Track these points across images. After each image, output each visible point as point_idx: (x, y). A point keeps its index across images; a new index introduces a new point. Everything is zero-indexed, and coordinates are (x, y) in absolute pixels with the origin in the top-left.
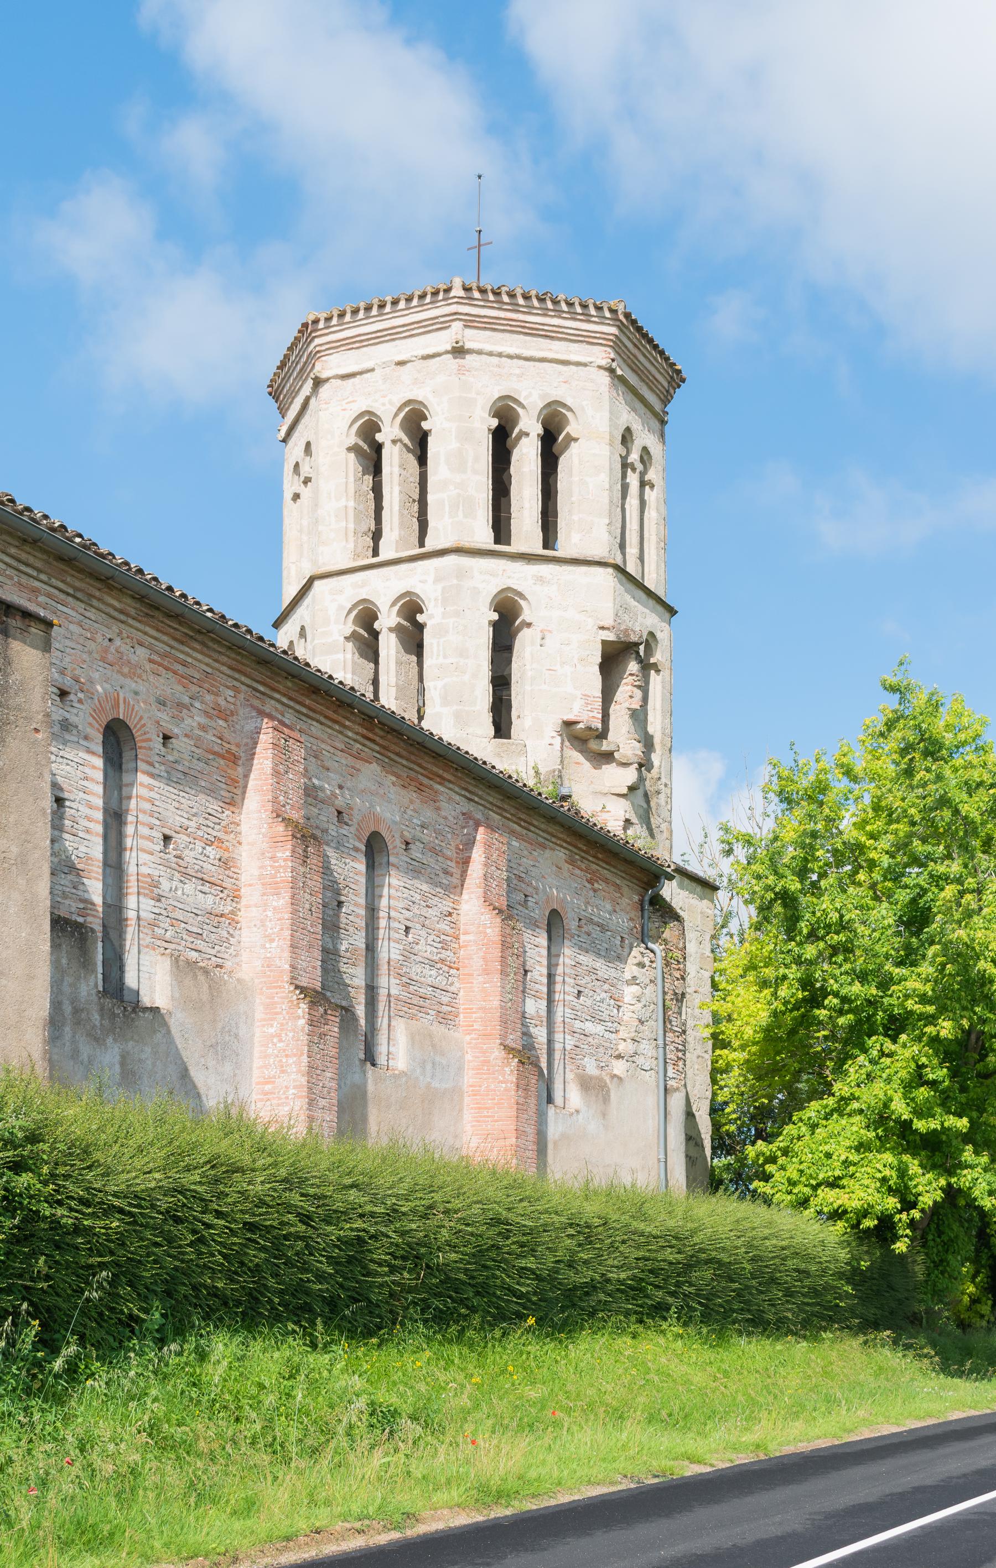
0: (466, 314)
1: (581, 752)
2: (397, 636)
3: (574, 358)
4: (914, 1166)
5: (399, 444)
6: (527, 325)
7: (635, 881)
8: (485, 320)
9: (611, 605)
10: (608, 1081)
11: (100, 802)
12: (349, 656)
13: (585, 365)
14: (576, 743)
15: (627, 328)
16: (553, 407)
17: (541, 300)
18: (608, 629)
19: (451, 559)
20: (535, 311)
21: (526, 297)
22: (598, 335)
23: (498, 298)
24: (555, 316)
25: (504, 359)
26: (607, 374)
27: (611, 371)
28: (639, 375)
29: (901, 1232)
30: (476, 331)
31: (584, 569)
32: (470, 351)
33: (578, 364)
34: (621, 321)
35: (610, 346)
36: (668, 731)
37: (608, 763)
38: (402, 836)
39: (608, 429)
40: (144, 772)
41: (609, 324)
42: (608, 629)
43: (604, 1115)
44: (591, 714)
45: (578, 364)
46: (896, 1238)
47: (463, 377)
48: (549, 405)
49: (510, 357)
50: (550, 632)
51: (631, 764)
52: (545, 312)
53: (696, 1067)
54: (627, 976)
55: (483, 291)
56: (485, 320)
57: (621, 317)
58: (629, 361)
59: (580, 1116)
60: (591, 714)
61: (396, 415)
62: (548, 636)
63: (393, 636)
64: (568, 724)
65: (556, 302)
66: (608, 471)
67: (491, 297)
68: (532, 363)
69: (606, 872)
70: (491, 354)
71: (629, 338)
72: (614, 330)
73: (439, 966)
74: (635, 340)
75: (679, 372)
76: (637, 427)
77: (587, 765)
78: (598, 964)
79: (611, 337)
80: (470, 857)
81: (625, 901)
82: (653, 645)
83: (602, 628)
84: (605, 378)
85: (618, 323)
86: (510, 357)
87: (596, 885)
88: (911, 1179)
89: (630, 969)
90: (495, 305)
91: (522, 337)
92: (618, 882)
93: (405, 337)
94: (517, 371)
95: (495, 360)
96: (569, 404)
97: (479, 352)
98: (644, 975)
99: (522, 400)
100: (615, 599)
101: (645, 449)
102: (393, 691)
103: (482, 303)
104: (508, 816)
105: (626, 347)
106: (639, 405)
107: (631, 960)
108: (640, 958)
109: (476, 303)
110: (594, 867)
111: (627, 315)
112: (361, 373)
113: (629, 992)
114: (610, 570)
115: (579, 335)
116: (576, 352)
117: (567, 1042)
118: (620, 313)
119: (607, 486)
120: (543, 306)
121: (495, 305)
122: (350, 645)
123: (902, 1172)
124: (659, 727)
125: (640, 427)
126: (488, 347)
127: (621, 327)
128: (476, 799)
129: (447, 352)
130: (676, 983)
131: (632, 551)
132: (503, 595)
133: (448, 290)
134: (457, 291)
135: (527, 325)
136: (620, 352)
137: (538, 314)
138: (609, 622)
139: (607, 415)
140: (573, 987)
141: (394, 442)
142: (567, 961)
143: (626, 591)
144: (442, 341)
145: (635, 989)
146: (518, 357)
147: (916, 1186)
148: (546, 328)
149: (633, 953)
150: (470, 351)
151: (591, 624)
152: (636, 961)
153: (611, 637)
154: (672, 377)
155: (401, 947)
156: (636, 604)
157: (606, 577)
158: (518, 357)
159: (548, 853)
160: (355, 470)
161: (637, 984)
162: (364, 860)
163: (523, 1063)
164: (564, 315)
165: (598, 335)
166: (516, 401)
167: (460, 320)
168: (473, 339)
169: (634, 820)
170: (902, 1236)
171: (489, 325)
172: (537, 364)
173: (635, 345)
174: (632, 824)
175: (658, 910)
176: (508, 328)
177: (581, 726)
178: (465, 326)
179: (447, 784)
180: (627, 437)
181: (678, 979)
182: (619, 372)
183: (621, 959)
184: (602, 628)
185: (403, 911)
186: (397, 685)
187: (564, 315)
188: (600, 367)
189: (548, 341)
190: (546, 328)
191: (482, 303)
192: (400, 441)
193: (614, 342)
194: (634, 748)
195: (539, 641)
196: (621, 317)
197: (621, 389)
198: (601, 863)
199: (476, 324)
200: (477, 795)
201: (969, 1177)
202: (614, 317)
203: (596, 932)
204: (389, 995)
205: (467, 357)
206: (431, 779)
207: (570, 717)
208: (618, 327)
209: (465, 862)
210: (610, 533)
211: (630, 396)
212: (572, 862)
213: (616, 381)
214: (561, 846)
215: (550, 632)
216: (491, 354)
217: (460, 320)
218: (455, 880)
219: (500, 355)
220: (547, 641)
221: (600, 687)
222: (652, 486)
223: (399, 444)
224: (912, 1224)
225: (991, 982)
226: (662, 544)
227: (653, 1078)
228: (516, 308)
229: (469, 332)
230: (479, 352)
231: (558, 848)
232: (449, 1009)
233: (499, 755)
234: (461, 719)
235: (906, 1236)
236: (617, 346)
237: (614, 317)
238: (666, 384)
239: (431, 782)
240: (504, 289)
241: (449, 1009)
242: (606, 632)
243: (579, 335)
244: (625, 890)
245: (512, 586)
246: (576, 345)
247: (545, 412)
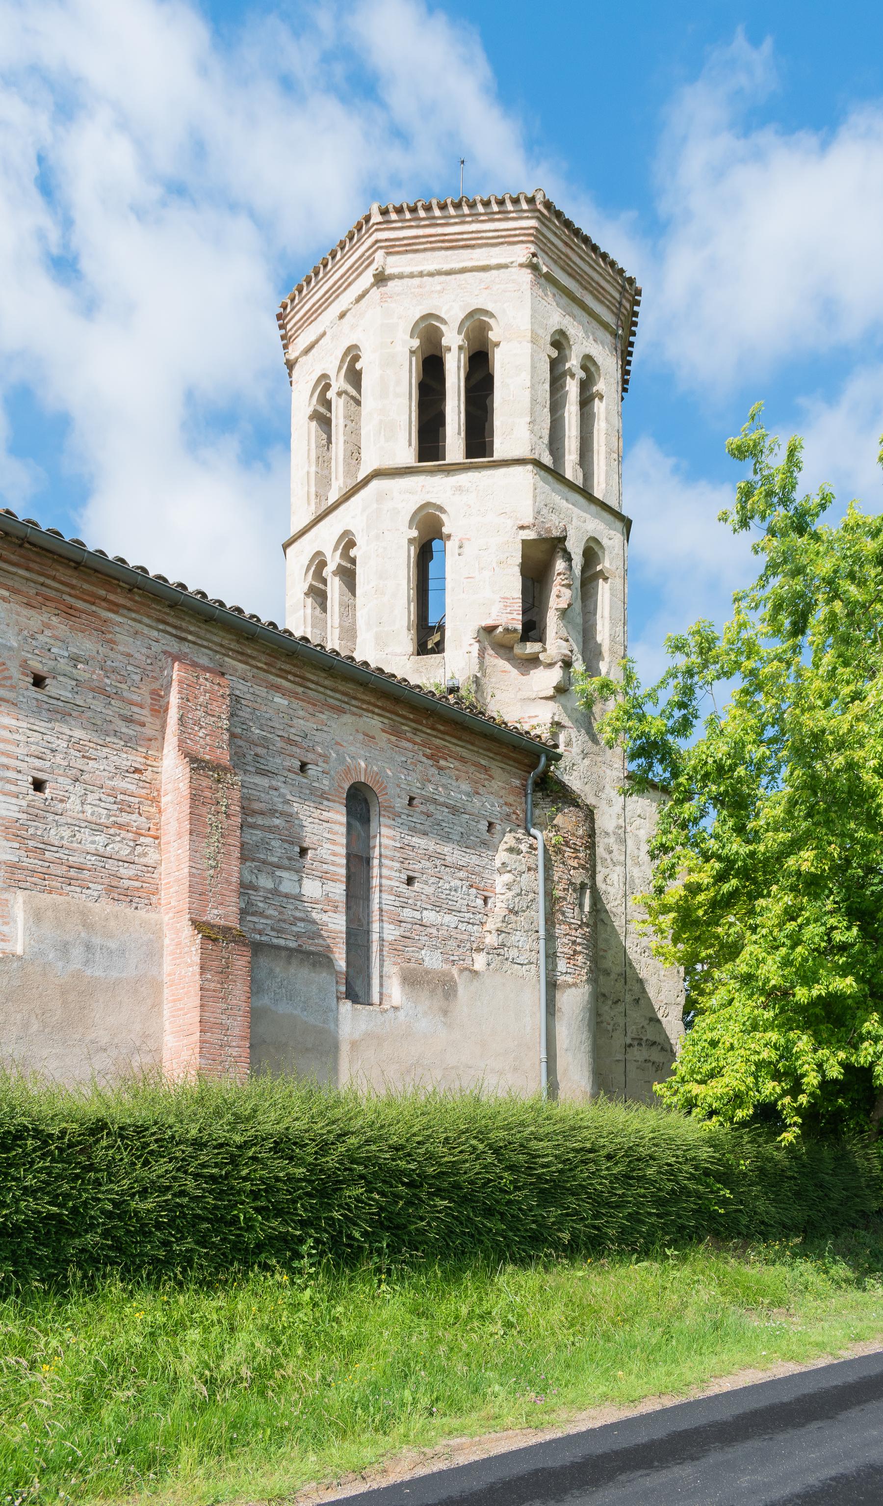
0: (386, 240)
1: (508, 660)
2: (341, 579)
3: (493, 262)
4: (804, 1042)
5: (344, 396)
6: (446, 238)
7: (511, 763)
8: (405, 242)
9: (530, 502)
10: (456, 976)
11: (343, 851)
12: (309, 611)
13: (505, 266)
14: (502, 651)
15: (549, 220)
16: (476, 317)
17: (457, 206)
18: (528, 527)
19: (375, 484)
20: (452, 221)
21: (443, 207)
22: (517, 232)
23: (415, 215)
24: (472, 222)
25: (426, 278)
26: (529, 271)
27: (534, 268)
28: (578, 281)
29: (788, 1121)
30: (397, 257)
31: (503, 471)
32: (391, 277)
33: (499, 267)
34: (539, 211)
35: (532, 242)
36: (620, 639)
37: (536, 668)
38: (24, 664)
39: (529, 327)
40: (386, 826)
41: (527, 218)
42: (528, 527)
43: (445, 1013)
44: (510, 616)
45: (499, 267)
46: (785, 1127)
47: (385, 305)
48: (471, 314)
49: (431, 274)
50: (469, 539)
51: (555, 663)
52: (462, 219)
53: (662, 973)
54: (498, 863)
55: (399, 210)
56: (405, 242)
57: (540, 207)
58: (562, 263)
59: (401, 1014)
60: (510, 616)
61: (340, 368)
62: (466, 544)
63: (337, 579)
64: (489, 630)
65: (472, 205)
66: (529, 369)
67: (408, 216)
68: (453, 276)
69: (458, 749)
70: (412, 276)
71: (555, 234)
72: (533, 223)
73: (112, 831)
74: (563, 237)
75: (631, 281)
76: (575, 331)
77: (514, 672)
78: (446, 849)
79: (531, 231)
80: (168, 703)
81: (496, 785)
82: (600, 553)
83: (522, 528)
84: (527, 276)
85: (537, 214)
86: (431, 274)
87: (442, 763)
88: (797, 1059)
89: (502, 856)
90: (413, 224)
91: (443, 252)
92: (483, 762)
93: (345, 289)
94: (439, 288)
95: (417, 281)
96: (489, 309)
97: (401, 276)
98: (519, 862)
99: (443, 315)
100: (535, 497)
101: (588, 358)
102: (337, 632)
103: (399, 225)
104: (260, 665)
105: (553, 244)
106: (577, 311)
107: (503, 846)
108: (512, 843)
109: (394, 225)
110: (438, 742)
111: (548, 205)
112: (317, 342)
113: (501, 881)
114: (530, 467)
115: (498, 237)
116: (496, 255)
117: (386, 931)
118: (538, 202)
119: (529, 384)
120: (460, 213)
121: (413, 224)
122: (309, 601)
123: (786, 1052)
124: (607, 635)
125: (581, 334)
126: (407, 270)
127: (541, 218)
128: (190, 637)
129: (373, 285)
130: (572, 872)
131: (571, 456)
132: (424, 513)
133: (368, 219)
134: (377, 218)
135: (446, 238)
136: (546, 249)
137: (456, 224)
138: (528, 520)
139: (528, 312)
140: (400, 872)
141: (339, 394)
142: (385, 841)
143: (553, 490)
144: (367, 278)
145: (507, 878)
146: (439, 273)
147: (802, 1066)
148: (465, 236)
149: (505, 839)
150: (391, 277)
151: (510, 525)
152: (507, 846)
153: (531, 535)
154: (623, 287)
155: (24, 803)
156: (570, 506)
157: (525, 475)
158: (439, 273)
159: (347, 718)
160: (317, 437)
161: (509, 872)
162: (344, 810)
163: (215, 940)
164: (482, 218)
165: (517, 232)
166: (438, 318)
167: (381, 248)
168: (395, 265)
169: (566, 721)
170: (790, 1125)
171: (409, 247)
172: (458, 276)
173: (566, 244)
174: (564, 727)
175: (548, 796)
176: (429, 246)
177: (500, 629)
178: (388, 254)
179: (122, 611)
180: (560, 341)
181: (575, 868)
182: (545, 269)
183: (487, 845)
184: (522, 528)
185: (27, 759)
186: (341, 626)
187: (482, 218)
188: (521, 265)
189: (469, 251)
190: (465, 236)
191: (399, 225)
192: (346, 392)
193: (535, 236)
194: (559, 647)
195: (457, 551)
196: (540, 207)
197: (550, 290)
198: (447, 738)
199: (397, 249)
200: (191, 633)
201: (871, 1050)
202: (532, 207)
203: (442, 814)
204: (382, 939)
205: (390, 284)
206: (93, 604)
207: (490, 622)
208: (538, 218)
209: (160, 710)
210: (532, 431)
211: (565, 300)
212: (396, 732)
213: (543, 280)
214: (373, 713)
215: (469, 539)
216: (412, 276)
217: (381, 248)
218: (148, 731)
219: (421, 275)
220: (465, 550)
221: (520, 587)
222: (601, 398)
223: (344, 396)
224: (798, 1111)
225: (874, 796)
226: (615, 456)
227: (533, 971)
228: (434, 221)
229: (391, 259)
230: (401, 276)
231: (366, 714)
232: (137, 884)
233: (417, 671)
234: (381, 642)
235: (795, 1124)
236: (538, 238)
237: (532, 207)
238: (617, 296)
239: (94, 608)
240: (419, 204)
241: (137, 884)
242: (527, 531)
243: (498, 237)
244: (496, 772)
245: (433, 501)
246: (497, 249)
247: (467, 324)
